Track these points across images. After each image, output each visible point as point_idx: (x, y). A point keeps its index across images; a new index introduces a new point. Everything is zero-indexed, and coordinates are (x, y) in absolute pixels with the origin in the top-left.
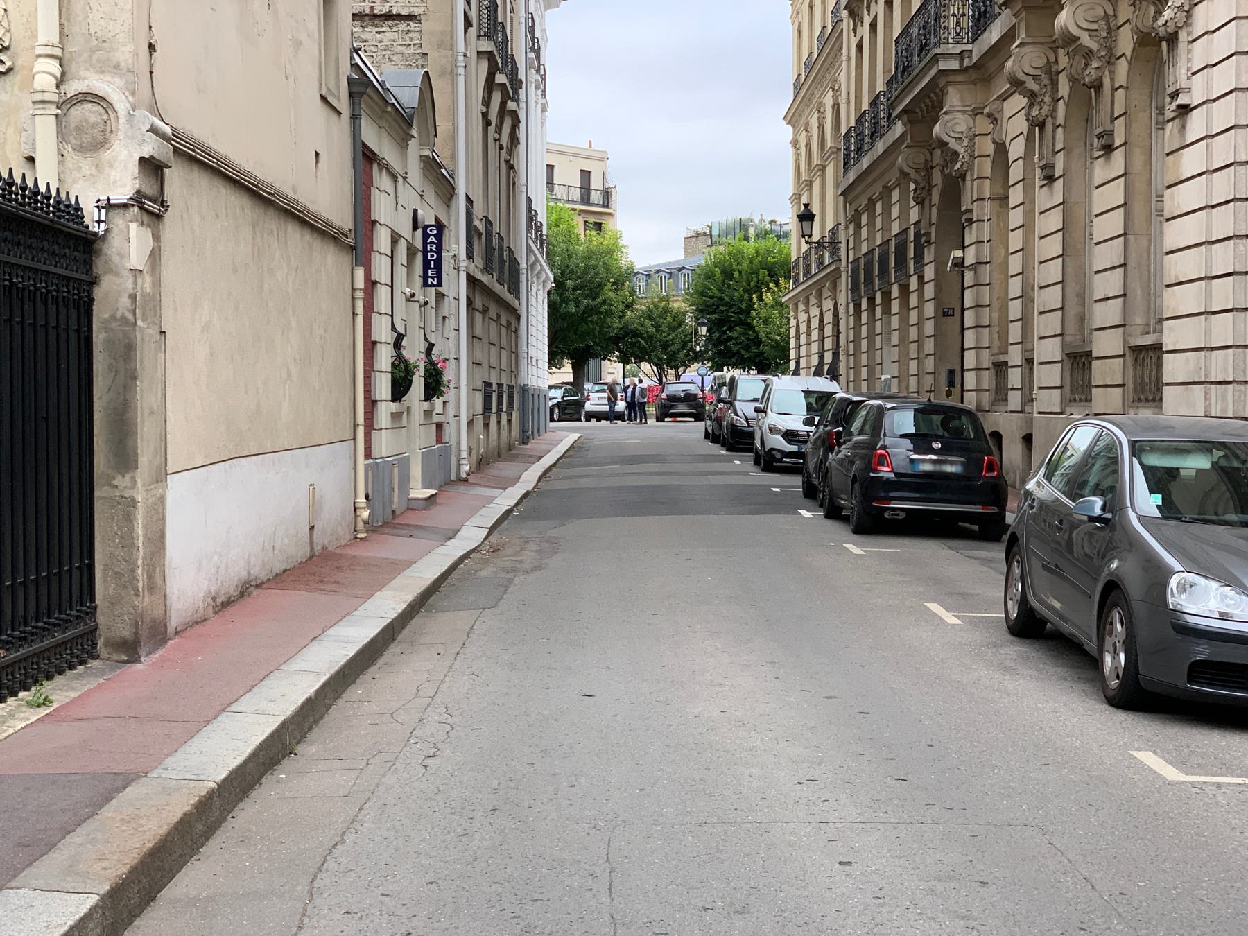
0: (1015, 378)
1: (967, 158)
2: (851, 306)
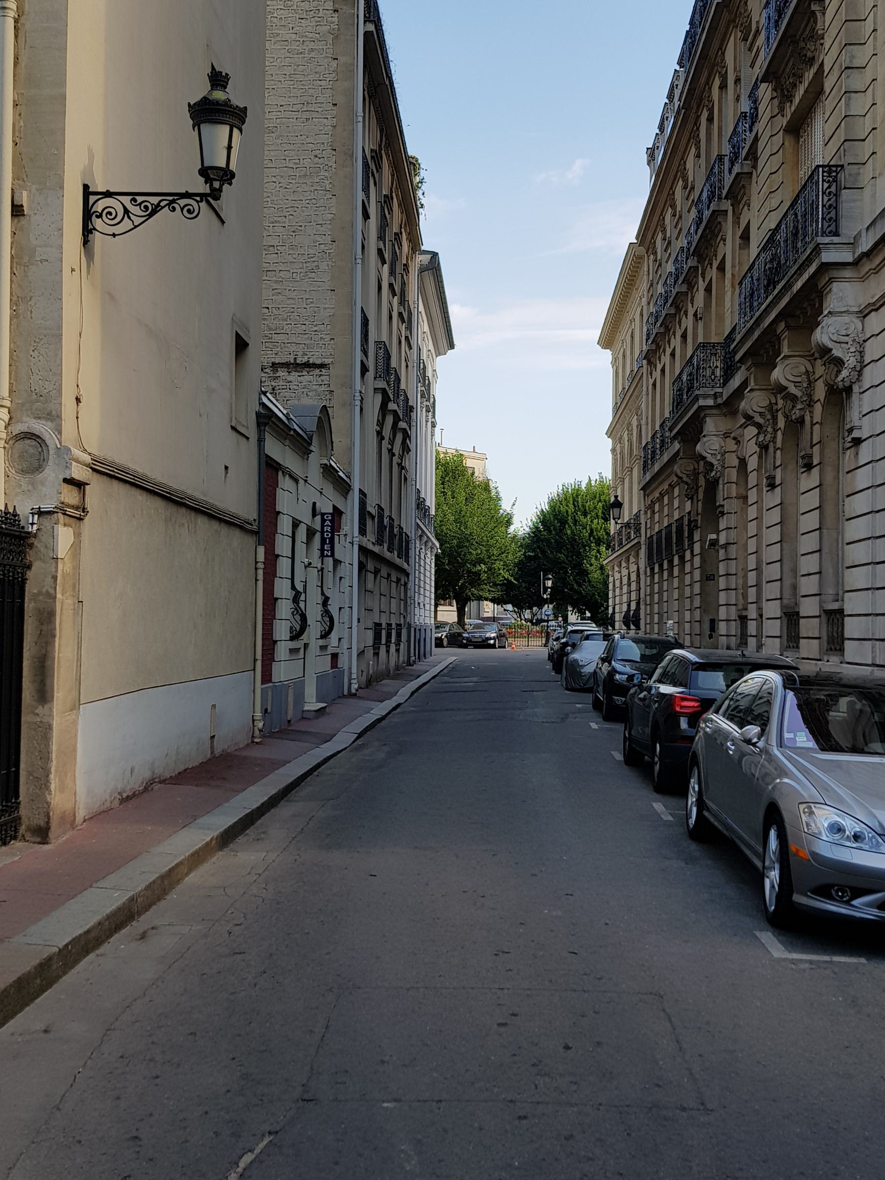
0: (752, 627)
1: (720, 468)
2: (648, 569)
